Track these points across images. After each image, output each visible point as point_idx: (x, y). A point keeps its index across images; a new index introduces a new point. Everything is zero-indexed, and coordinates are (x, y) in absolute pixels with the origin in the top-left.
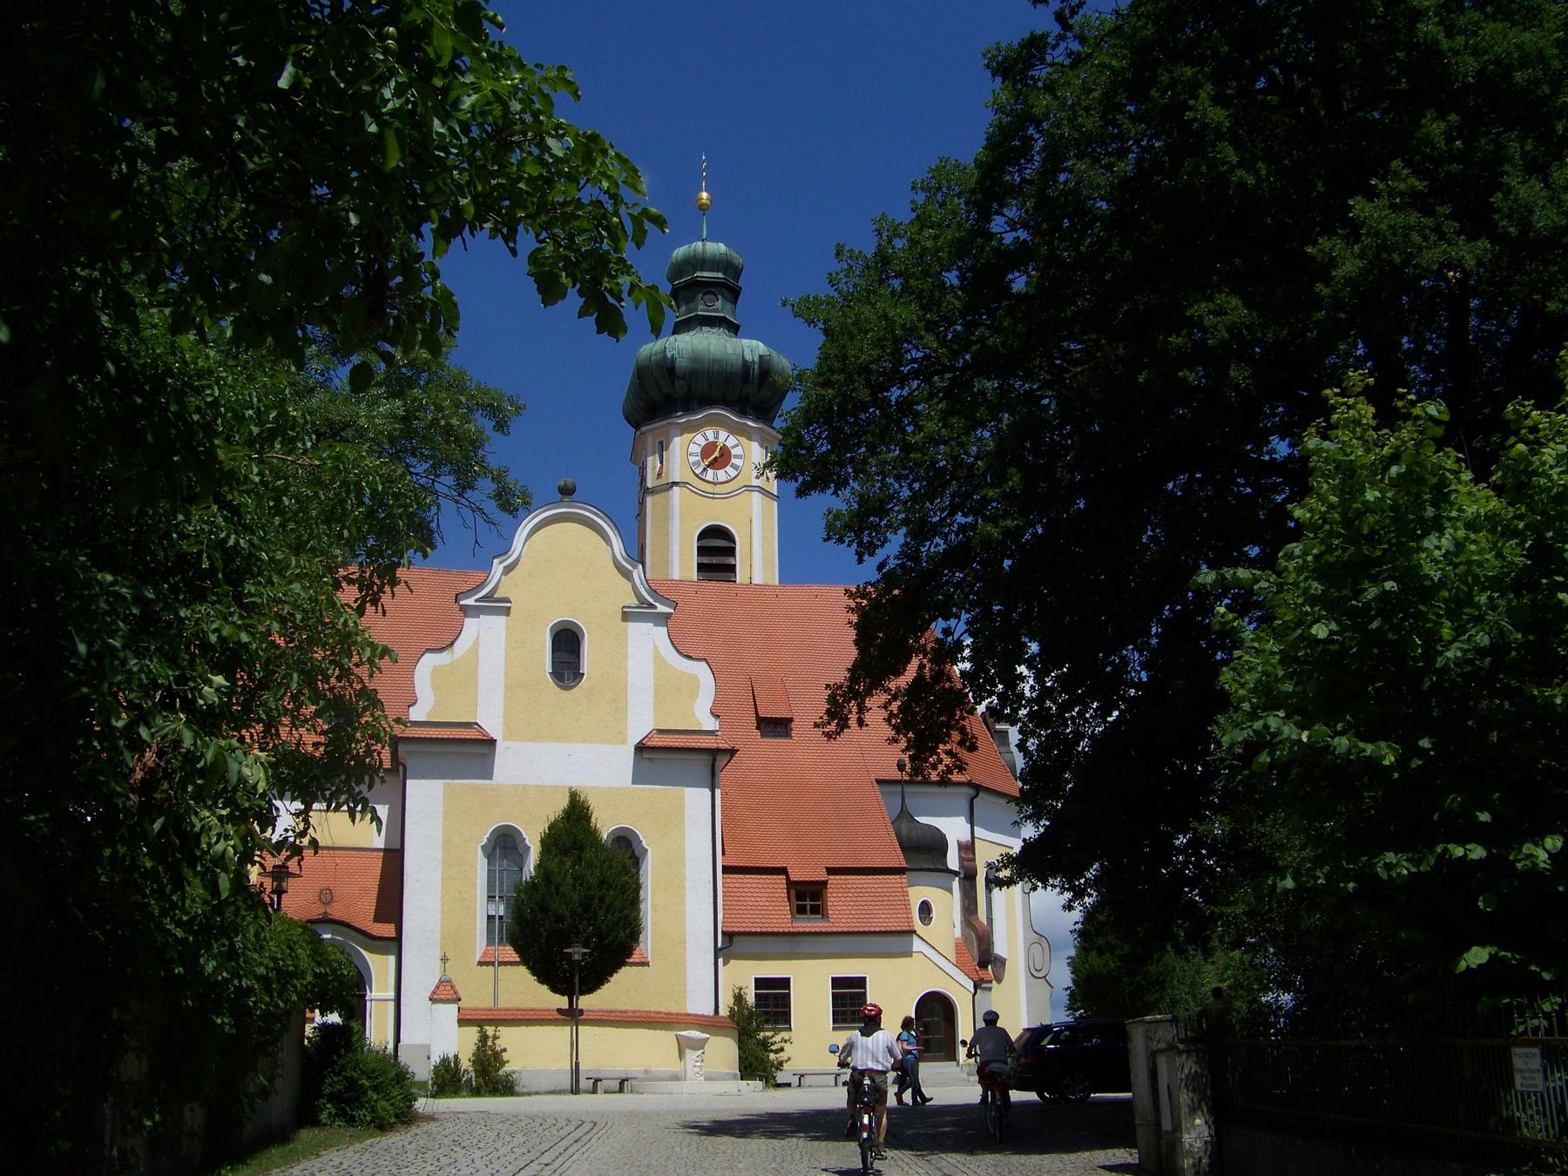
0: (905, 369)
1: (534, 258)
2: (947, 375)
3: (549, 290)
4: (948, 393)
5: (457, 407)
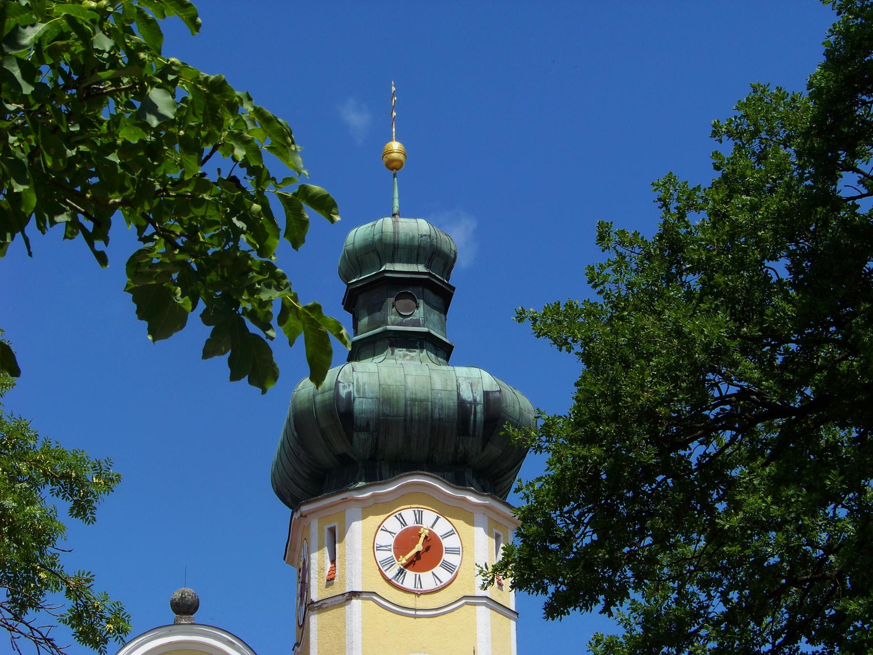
0: (712, 414)
1: (136, 265)
2: (779, 421)
3: (157, 312)
4: (779, 449)
5: (13, 479)
